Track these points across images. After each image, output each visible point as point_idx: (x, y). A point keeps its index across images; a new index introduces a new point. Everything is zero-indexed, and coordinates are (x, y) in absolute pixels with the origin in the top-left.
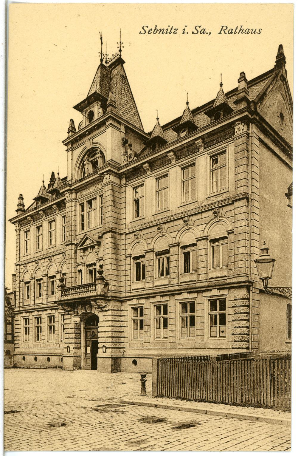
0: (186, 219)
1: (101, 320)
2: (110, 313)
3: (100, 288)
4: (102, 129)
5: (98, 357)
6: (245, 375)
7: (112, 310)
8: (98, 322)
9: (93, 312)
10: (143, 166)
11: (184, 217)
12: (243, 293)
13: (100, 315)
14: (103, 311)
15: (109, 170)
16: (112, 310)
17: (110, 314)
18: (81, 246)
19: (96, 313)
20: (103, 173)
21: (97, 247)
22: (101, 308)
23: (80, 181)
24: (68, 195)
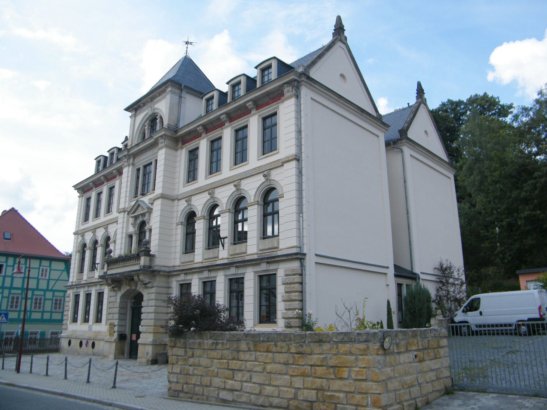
0: (265, 173)
1: (145, 298)
2: (153, 290)
3: (143, 261)
4: (164, 95)
5: (141, 344)
6: (492, 371)
7: (157, 287)
8: (142, 301)
9: (138, 289)
10: (247, 105)
11: (264, 171)
12: (295, 265)
13: (145, 293)
14: (147, 288)
15: (164, 135)
16: (157, 287)
17: (154, 291)
18: (134, 213)
19: (141, 291)
20: (158, 138)
21: (147, 215)
22: (145, 284)
23: (137, 145)
24: (126, 160)
